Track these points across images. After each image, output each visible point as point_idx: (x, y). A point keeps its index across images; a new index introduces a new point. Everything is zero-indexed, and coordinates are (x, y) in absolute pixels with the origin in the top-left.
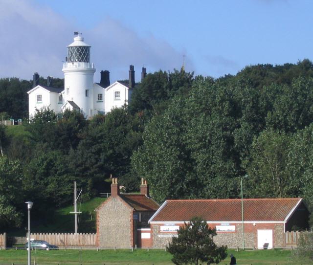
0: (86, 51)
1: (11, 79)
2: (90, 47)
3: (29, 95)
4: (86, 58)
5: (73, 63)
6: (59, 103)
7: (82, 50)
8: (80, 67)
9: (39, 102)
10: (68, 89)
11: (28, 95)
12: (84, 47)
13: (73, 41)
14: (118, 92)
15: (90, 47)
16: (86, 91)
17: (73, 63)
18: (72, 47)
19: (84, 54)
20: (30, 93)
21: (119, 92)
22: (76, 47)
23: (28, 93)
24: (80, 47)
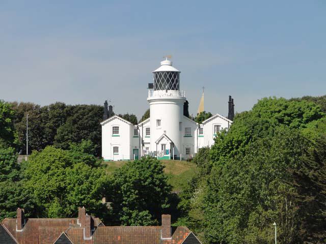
0: (175, 77)
1: (22, 104)
2: (180, 72)
3: (102, 127)
4: (175, 85)
5: (167, 92)
6: (134, 137)
7: (170, 76)
8: (316, 124)
9: (114, 135)
10: (159, 121)
11: (101, 127)
12: (173, 72)
13: (160, 66)
14: (116, 127)
15: (180, 72)
16: (180, 123)
17: (167, 92)
18: (158, 72)
19: (173, 81)
20: (103, 125)
21: (118, 127)
22: (163, 72)
23: (102, 123)
24: (168, 72)
